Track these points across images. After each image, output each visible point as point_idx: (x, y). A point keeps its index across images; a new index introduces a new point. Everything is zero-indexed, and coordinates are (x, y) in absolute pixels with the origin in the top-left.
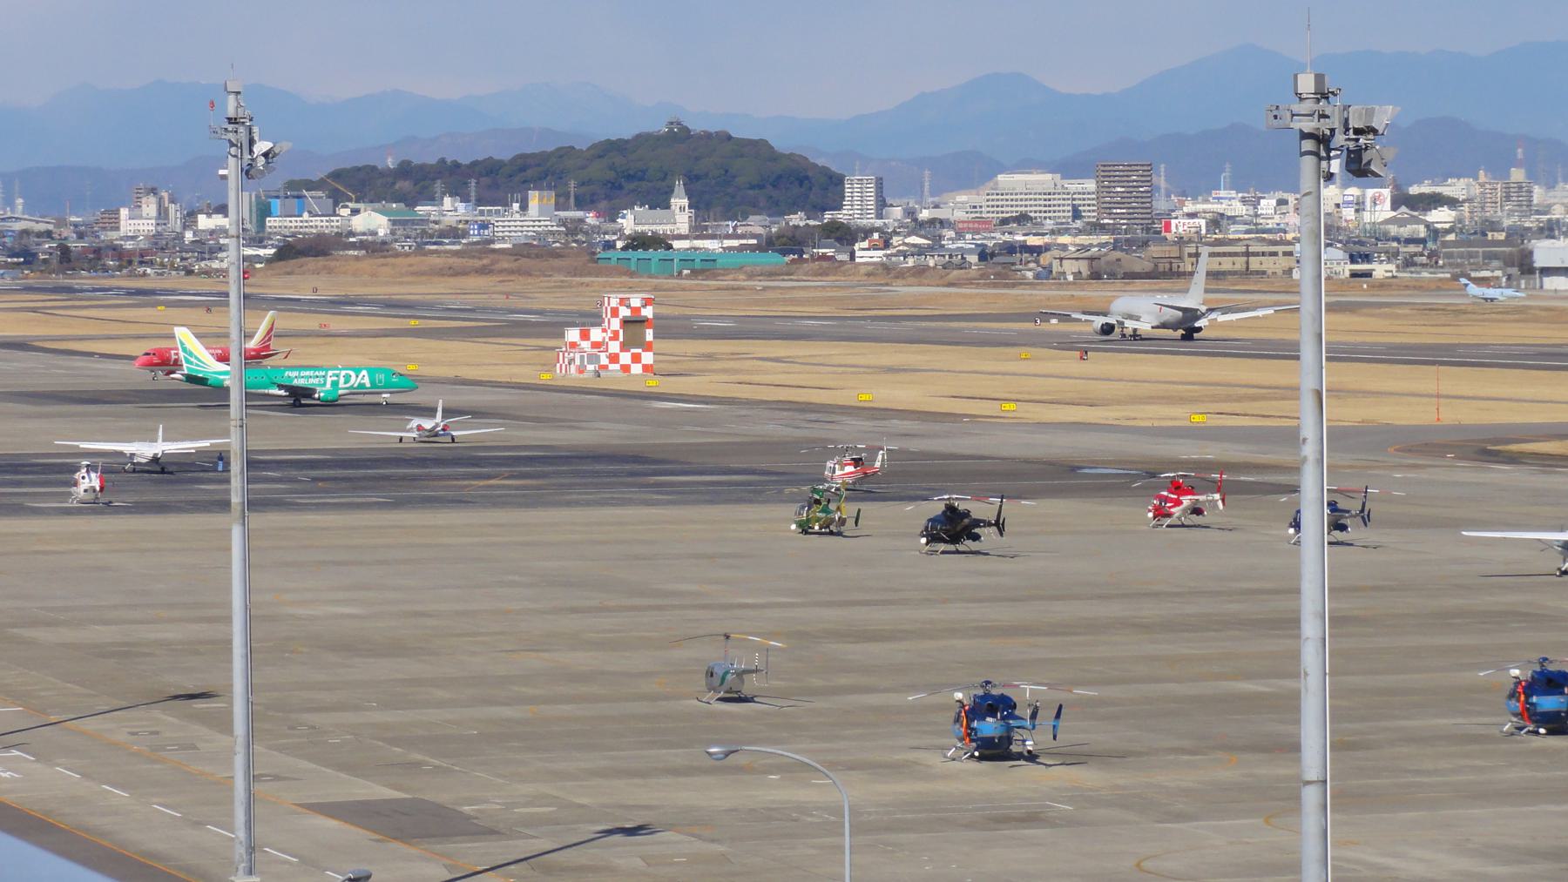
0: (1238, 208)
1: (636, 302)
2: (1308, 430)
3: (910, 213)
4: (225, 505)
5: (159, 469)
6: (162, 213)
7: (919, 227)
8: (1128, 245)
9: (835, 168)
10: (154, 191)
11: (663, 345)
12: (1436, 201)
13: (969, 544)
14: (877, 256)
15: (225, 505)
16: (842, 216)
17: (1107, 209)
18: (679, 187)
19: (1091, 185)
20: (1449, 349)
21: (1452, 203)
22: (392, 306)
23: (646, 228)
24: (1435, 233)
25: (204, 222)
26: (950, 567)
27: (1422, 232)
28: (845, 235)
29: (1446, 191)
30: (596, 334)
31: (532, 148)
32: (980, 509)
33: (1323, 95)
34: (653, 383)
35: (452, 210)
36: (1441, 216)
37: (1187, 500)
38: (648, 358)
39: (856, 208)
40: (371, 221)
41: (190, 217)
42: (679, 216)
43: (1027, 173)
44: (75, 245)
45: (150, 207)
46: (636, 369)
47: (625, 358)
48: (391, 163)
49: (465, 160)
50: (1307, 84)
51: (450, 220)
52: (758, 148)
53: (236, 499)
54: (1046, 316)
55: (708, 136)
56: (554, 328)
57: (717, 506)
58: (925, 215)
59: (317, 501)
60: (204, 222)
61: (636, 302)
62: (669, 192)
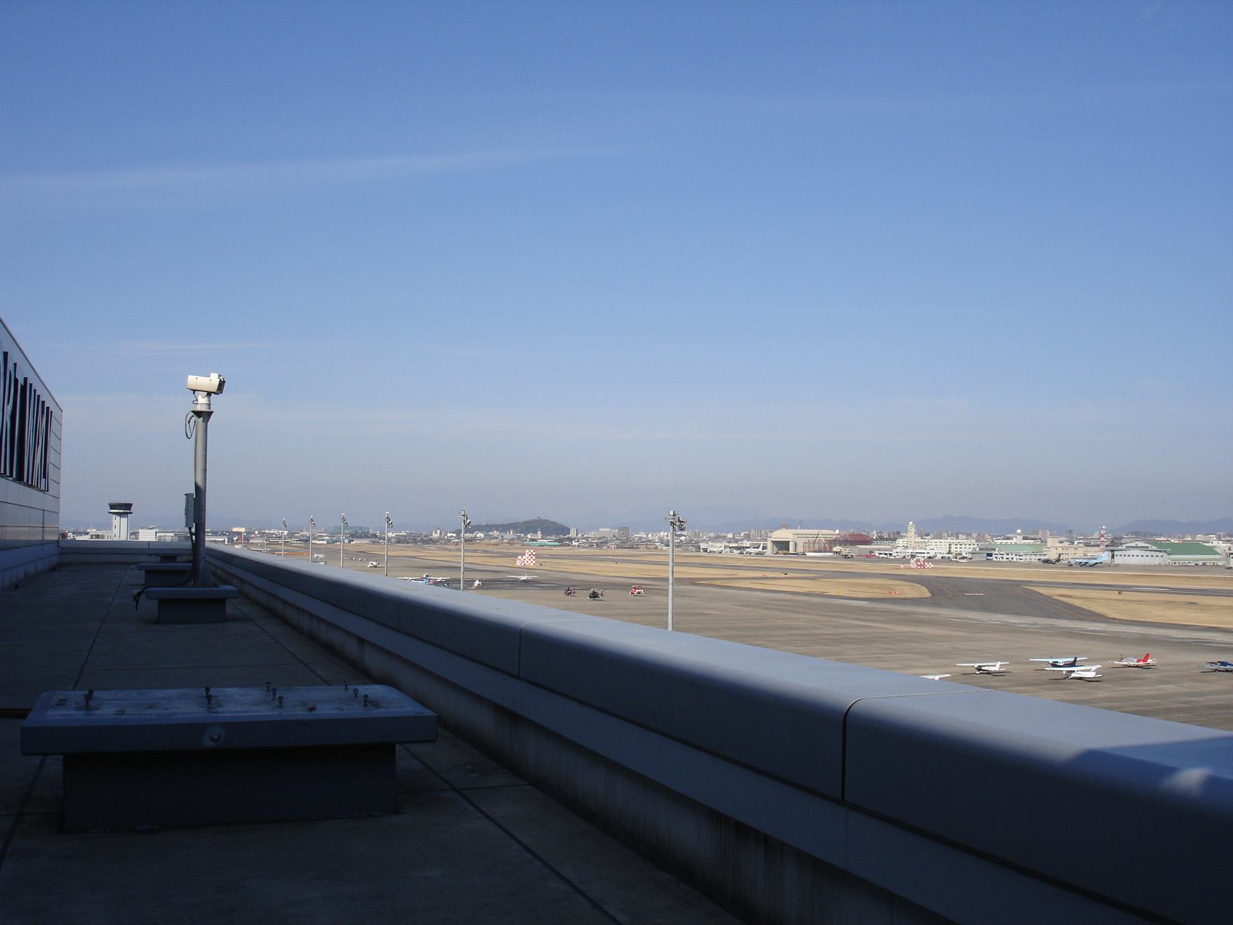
0: (645, 536)
1: (532, 551)
2: (670, 578)
3: (583, 536)
4: (460, 589)
5: (608, 595)
6: (441, 533)
7: (585, 538)
8: (623, 542)
9: (569, 527)
10: (439, 528)
11: (537, 560)
12: (682, 535)
13: (597, 599)
14: (577, 544)
15: (460, 589)
16: (570, 536)
17: (619, 535)
18: (539, 530)
19: (617, 531)
20: (1220, 628)
21: (685, 536)
22: (485, 552)
23: (533, 538)
24: (681, 541)
25: (449, 535)
26: (594, 603)
27: (679, 541)
28: (571, 540)
29: (684, 533)
30: (524, 557)
31: (511, 522)
32: (599, 592)
33: (674, 515)
34: (535, 567)
35: (496, 533)
36: (683, 538)
37: (637, 591)
38: (534, 562)
39: (572, 534)
40: (480, 535)
41: (446, 534)
42: (539, 535)
43: (1002, 580)
44: (424, 539)
45: (438, 532)
46: (532, 564)
47: (530, 562)
48: (485, 524)
49: (498, 524)
50: (672, 513)
51: (495, 535)
52: (554, 523)
53: (462, 587)
54: (609, 556)
55: (544, 520)
56: (516, 555)
57: (249, 558)
58: (585, 536)
59: (921, 629)
60: (449, 535)
61: (532, 551)
62: (537, 531)
